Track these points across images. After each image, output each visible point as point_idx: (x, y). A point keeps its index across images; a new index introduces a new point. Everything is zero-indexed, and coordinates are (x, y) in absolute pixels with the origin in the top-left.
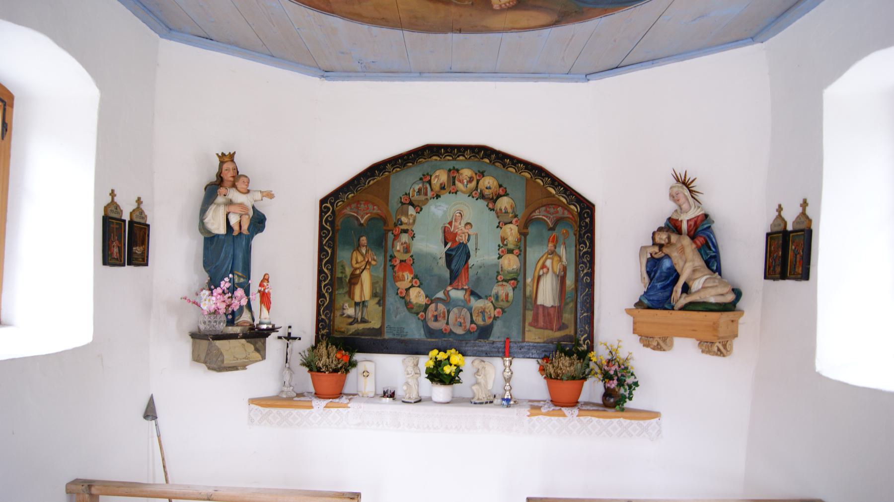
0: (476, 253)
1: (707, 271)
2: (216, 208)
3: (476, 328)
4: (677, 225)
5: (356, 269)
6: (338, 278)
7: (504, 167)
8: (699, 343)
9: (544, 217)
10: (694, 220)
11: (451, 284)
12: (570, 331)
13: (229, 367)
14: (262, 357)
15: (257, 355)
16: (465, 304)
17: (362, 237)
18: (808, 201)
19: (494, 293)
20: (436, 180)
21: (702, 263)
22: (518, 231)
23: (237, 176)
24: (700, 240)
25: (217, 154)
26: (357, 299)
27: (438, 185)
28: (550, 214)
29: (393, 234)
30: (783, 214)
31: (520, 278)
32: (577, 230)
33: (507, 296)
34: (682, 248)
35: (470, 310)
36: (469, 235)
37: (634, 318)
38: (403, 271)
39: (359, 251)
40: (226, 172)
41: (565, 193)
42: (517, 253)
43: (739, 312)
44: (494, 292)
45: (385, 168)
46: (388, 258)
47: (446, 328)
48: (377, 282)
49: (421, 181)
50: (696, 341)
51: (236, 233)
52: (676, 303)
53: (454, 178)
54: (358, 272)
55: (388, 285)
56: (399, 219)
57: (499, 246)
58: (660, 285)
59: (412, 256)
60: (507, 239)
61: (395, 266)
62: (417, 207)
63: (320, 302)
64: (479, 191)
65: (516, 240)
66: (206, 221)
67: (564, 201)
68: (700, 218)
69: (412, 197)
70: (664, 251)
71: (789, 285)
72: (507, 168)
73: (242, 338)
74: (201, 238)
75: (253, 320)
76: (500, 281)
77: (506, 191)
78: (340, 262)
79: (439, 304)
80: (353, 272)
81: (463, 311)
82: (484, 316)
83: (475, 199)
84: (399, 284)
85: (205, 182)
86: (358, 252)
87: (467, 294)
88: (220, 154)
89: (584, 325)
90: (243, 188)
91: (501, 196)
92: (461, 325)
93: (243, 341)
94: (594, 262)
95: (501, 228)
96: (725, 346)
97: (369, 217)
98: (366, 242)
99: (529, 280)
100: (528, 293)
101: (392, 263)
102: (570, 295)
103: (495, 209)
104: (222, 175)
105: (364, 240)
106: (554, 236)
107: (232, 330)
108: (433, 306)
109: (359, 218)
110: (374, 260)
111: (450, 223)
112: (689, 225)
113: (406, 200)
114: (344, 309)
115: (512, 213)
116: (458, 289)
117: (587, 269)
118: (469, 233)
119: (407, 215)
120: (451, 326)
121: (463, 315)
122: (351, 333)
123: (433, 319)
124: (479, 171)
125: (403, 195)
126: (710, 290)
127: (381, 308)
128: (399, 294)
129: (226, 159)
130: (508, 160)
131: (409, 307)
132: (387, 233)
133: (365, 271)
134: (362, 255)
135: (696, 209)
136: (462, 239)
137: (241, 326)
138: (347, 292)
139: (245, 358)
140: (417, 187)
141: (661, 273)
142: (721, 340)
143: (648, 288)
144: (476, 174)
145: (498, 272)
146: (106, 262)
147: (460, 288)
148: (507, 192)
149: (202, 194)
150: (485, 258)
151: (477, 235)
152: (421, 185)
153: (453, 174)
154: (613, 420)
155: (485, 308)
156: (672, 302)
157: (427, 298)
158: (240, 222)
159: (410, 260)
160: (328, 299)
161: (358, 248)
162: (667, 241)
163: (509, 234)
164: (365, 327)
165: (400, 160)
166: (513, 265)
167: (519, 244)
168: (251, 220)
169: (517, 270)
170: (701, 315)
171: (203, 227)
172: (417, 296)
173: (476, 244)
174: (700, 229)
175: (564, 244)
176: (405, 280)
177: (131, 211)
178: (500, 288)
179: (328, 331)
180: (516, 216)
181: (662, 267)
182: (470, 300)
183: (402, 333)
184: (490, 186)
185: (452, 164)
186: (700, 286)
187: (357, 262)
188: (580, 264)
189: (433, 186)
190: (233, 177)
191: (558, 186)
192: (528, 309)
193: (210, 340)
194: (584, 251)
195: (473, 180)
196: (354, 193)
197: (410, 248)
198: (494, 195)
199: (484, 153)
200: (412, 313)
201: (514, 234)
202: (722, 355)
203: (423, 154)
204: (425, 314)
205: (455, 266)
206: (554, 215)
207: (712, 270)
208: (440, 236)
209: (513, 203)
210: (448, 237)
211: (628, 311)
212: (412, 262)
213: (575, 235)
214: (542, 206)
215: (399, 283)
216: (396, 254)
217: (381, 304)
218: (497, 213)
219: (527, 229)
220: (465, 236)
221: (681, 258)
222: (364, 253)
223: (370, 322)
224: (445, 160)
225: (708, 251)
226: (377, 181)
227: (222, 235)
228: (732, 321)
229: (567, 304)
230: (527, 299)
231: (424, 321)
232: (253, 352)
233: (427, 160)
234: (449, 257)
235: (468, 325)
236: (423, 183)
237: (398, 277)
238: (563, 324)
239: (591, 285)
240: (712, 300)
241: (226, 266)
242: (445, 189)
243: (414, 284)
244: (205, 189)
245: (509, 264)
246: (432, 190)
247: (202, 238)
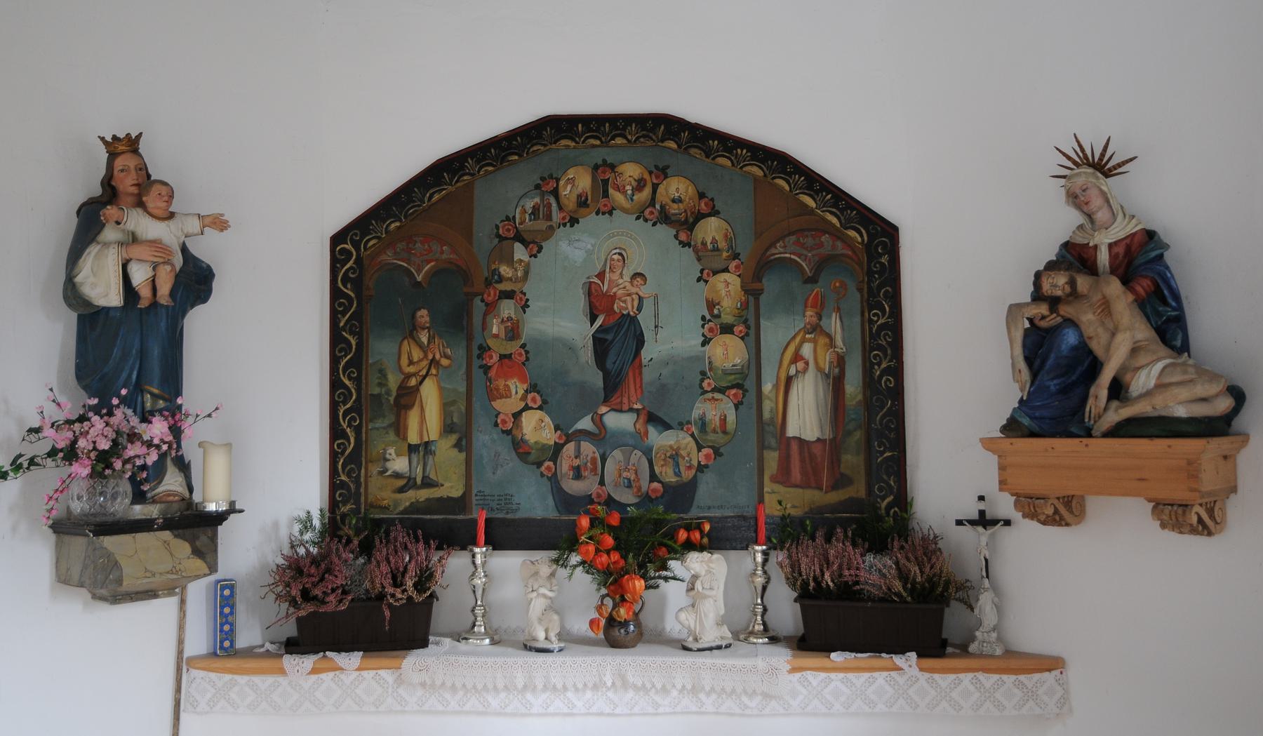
0: (656, 335)
1: (1163, 350)
2: (99, 250)
3: (662, 489)
4: (1085, 256)
5: (408, 376)
6: (372, 395)
7: (707, 157)
8: (1154, 508)
9: (793, 257)
10: (1123, 244)
11: (606, 401)
12: (858, 490)
13: (137, 593)
14: (210, 568)
15: (198, 564)
16: (637, 442)
17: (420, 309)
19: (697, 416)
20: (569, 188)
21: (1152, 334)
22: (742, 287)
23: (146, 182)
24: (1143, 286)
25: (102, 139)
26: (413, 438)
27: (574, 198)
28: (806, 249)
29: (482, 301)
31: (750, 384)
32: (863, 281)
33: (723, 420)
34: (1103, 303)
35: (647, 452)
36: (641, 299)
37: (999, 456)
38: (507, 376)
39: (414, 339)
40: (122, 175)
41: (835, 205)
42: (741, 331)
43: (1240, 438)
44: (696, 414)
45: (462, 167)
46: (476, 352)
47: (600, 492)
48: (453, 403)
49: (538, 191)
50: (1009, 496)
51: (143, 304)
52: (1095, 422)
53: (605, 182)
54: (413, 382)
55: (477, 406)
56: (495, 269)
57: (703, 318)
59: (523, 346)
60: (718, 304)
61: (490, 367)
62: (531, 246)
63: (336, 447)
64: (658, 207)
65: (739, 305)
66: (78, 279)
67: (835, 220)
68: (1136, 239)
69: (521, 223)
72: (713, 159)
73: (162, 528)
74: (71, 318)
75: (191, 490)
76: (707, 392)
77: (714, 206)
78: (374, 363)
79: (582, 442)
80: (403, 381)
81: (633, 455)
82: (677, 465)
83: (650, 223)
84: (498, 404)
85: (81, 198)
86: (411, 340)
87: (641, 421)
88: (109, 139)
89: (885, 477)
90: (158, 208)
91: (704, 216)
92: (629, 486)
93: (167, 535)
94: (902, 347)
95: (706, 282)
96: (1211, 512)
97: (432, 267)
98: (428, 319)
99: (767, 387)
100: (766, 415)
101: (484, 362)
102: (853, 416)
103: (692, 243)
104: (113, 183)
105: (423, 315)
106: (817, 294)
107: (139, 511)
108: (570, 448)
109: (414, 271)
110: (447, 357)
111: (601, 276)
112: (1113, 254)
113: (508, 230)
114: (386, 460)
115: (728, 251)
116: (620, 411)
117: (887, 361)
118: (641, 294)
119: (510, 261)
120: (609, 488)
121: (634, 465)
122: (401, 508)
123: (571, 473)
124: (656, 167)
125: (502, 221)
126: (1176, 390)
127: (463, 455)
128: (500, 426)
129: (121, 148)
130: (716, 142)
131: (521, 451)
132: (472, 300)
133: (427, 380)
134: (420, 346)
135: (1127, 220)
136: (627, 308)
137: (160, 502)
138: (393, 423)
139: (171, 572)
140: (529, 204)
142: (1204, 501)
143: (1029, 392)
144: (651, 173)
145: (703, 373)
147: (625, 407)
148: (716, 208)
149: (71, 224)
150: (674, 344)
151: (656, 297)
152: (537, 200)
153: (604, 175)
154: (962, 676)
155: (679, 448)
156: (1086, 420)
157: (559, 432)
158: (153, 281)
159: (520, 355)
160: (352, 440)
161: (411, 332)
162: (1068, 289)
163: (723, 293)
164: (431, 497)
165: (493, 151)
166: (734, 359)
167: (745, 313)
168: (177, 276)
169: (743, 366)
170: (1161, 444)
171: (72, 294)
172: (538, 428)
173: (656, 316)
174: (1141, 260)
175: (839, 309)
176: (510, 397)
178: (708, 405)
179: (354, 506)
180: (736, 256)
182: (646, 433)
183: (510, 506)
184: (680, 197)
185: (599, 155)
186: (1152, 383)
187: (411, 363)
188: (872, 349)
189: (564, 201)
190: (138, 185)
191: (821, 191)
192: (770, 448)
193: (88, 536)
194: (878, 323)
195: (645, 186)
196: (400, 221)
197: (521, 327)
198: (689, 214)
199: (665, 128)
200: (526, 462)
201: (732, 293)
202: (1206, 532)
203: (540, 136)
204: (555, 464)
205: (615, 363)
206: (814, 252)
207: (1172, 348)
208: (581, 302)
209: (730, 230)
210: (597, 304)
211: (988, 443)
212: (524, 358)
213: (860, 290)
214: (790, 234)
215: (498, 401)
216: (491, 342)
217: (464, 448)
218: (696, 251)
219: (761, 282)
220: (633, 300)
221: (1103, 324)
222: (426, 343)
223: (442, 485)
224: (586, 148)
225: (1161, 309)
226: (447, 195)
227: (115, 308)
228: (1225, 457)
229: (849, 433)
230: (767, 428)
231: (554, 480)
232: (189, 558)
233: (548, 148)
234: (601, 345)
235: (645, 483)
236: (542, 195)
237: (497, 390)
238: (842, 475)
239: (898, 393)
240: (1181, 412)
241: (124, 375)
242: (588, 206)
243: (531, 404)
244: (78, 212)
245: (726, 355)
246: (560, 208)
247: (73, 316)
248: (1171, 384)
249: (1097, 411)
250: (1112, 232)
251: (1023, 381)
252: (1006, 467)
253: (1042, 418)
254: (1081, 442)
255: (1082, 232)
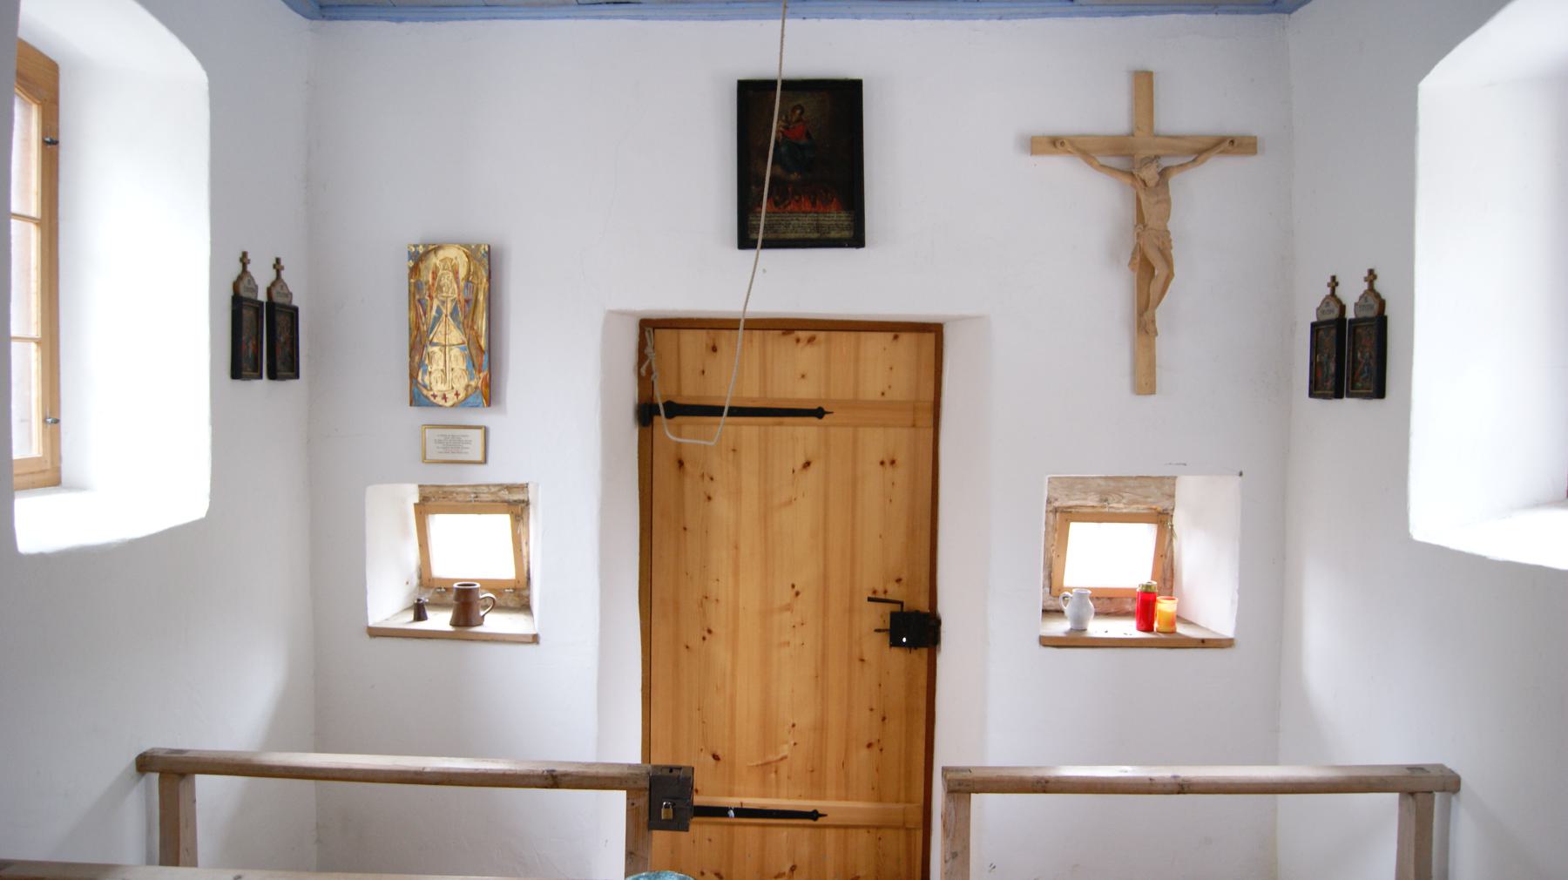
18: (1376, 272)
30: (1339, 292)
71: (1350, 408)
146: (236, 373)
177: (269, 284)
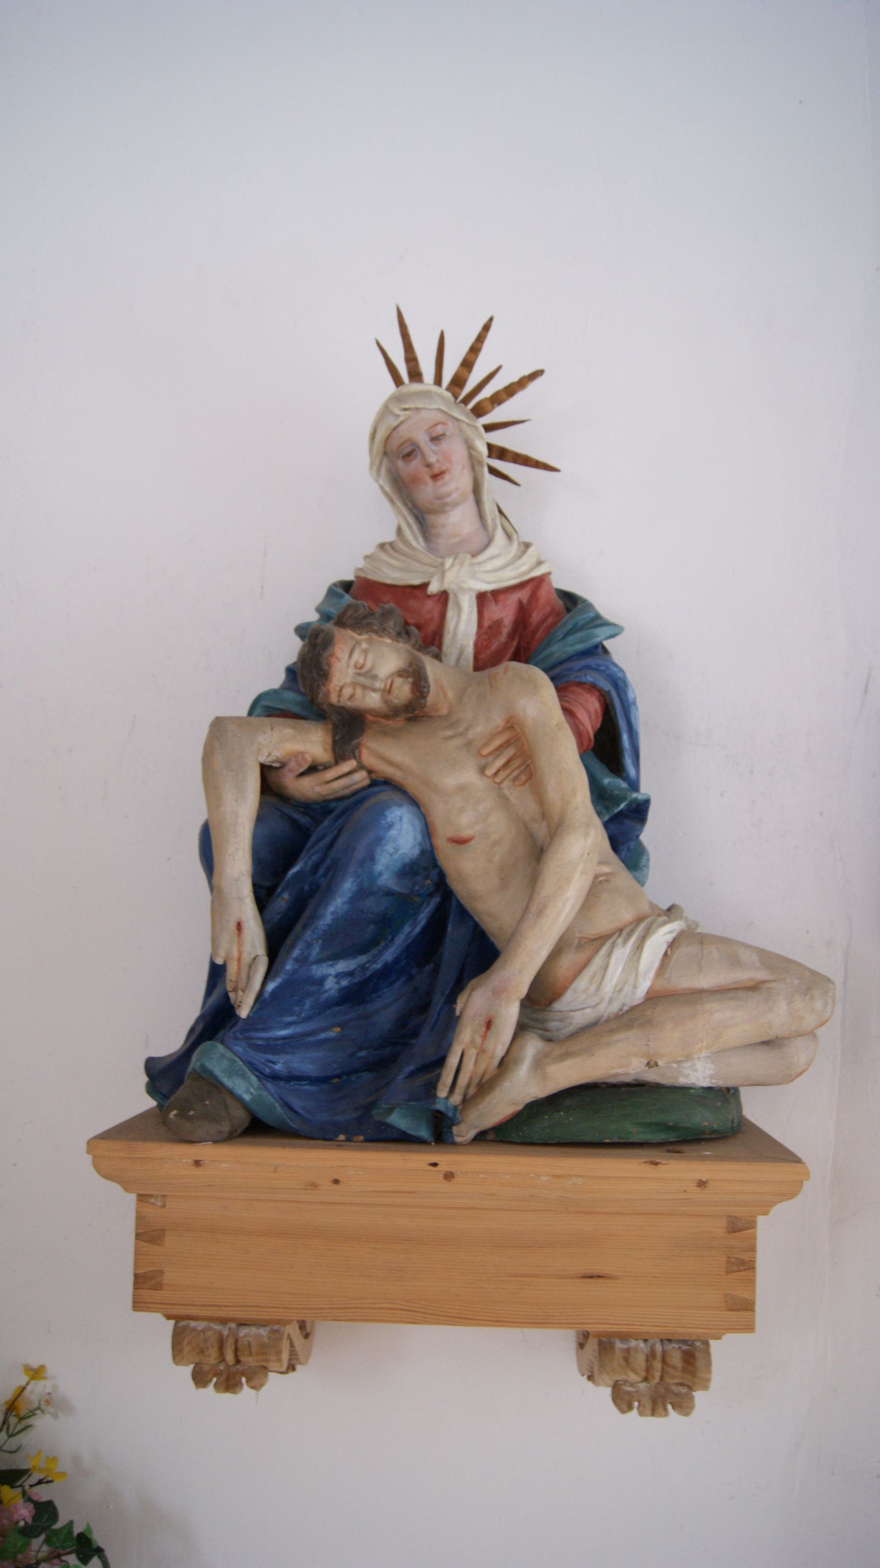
10: (513, 600)
37: (142, 1198)
52: (465, 1101)
58: (339, 976)
70: (368, 758)
112: (486, 623)
141: (361, 894)
149: (236, 931)
156: (442, 1092)
157: (559, 603)
181: (371, 858)
248: (696, 996)
249: (482, 1067)
250: (489, 566)
251: (247, 958)
252: (164, 1230)
253: (292, 1078)
254: (435, 1165)
255: (395, 554)
